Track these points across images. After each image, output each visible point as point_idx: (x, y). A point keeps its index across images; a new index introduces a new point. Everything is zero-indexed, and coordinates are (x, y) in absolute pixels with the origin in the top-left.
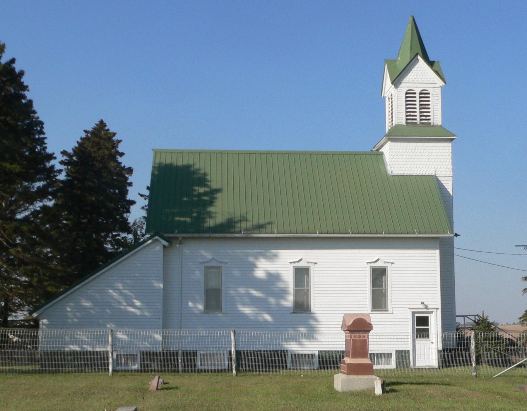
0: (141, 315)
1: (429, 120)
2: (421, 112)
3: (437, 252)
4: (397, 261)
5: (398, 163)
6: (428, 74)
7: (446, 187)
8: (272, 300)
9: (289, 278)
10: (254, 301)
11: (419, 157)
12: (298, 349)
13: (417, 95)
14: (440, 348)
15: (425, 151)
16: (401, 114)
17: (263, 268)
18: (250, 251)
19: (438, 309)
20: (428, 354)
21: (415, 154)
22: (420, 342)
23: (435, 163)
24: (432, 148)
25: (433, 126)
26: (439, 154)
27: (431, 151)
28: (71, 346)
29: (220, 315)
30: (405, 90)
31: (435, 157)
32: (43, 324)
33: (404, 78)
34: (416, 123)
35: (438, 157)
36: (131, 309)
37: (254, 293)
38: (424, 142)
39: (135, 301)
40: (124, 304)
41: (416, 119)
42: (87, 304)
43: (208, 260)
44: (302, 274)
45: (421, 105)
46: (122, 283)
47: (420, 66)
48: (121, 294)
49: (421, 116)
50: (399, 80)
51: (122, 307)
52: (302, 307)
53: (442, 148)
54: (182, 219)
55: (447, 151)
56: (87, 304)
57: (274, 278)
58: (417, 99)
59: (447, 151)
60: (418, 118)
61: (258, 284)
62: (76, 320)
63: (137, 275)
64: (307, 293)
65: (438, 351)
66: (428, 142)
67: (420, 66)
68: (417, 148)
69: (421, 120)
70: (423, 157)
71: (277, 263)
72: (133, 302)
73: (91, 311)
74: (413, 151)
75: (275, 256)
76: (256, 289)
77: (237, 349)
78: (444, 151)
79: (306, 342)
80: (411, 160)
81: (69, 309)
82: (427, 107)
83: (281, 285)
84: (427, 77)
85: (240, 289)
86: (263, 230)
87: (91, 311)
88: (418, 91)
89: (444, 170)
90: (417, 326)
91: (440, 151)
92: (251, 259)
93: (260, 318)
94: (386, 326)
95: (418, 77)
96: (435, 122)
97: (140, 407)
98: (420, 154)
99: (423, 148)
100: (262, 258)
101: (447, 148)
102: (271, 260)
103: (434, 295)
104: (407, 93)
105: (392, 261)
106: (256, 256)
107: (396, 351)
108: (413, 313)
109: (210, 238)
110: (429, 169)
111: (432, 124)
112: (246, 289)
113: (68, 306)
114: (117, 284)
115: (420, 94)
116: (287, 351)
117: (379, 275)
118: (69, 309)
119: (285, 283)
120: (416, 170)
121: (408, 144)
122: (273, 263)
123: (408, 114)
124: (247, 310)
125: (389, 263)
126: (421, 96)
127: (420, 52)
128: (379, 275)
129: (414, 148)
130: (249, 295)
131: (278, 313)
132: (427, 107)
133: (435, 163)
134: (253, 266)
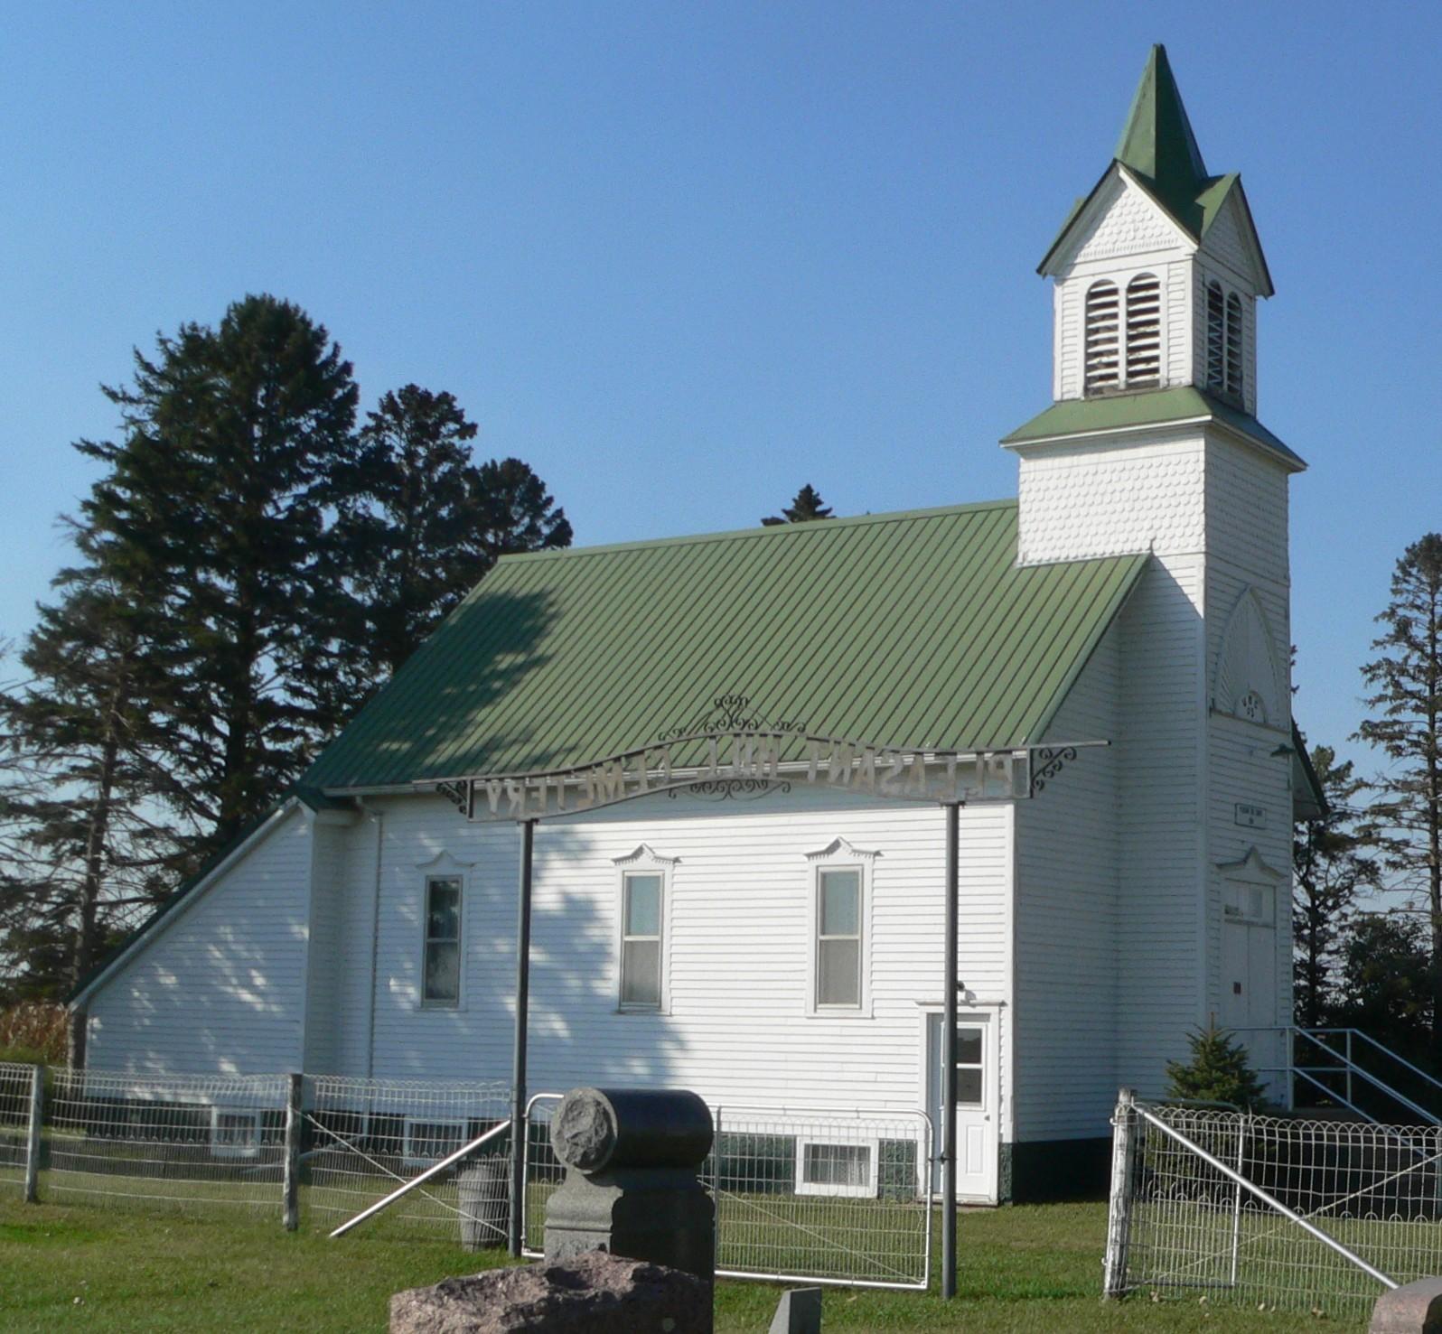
0: (264, 1011)
1: (1156, 371)
2: (1131, 350)
4: (892, 845)
5: (1042, 526)
6: (1151, 224)
7: (1186, 590)
8: (573, 982)
9: (611, 906)
13: (1121, 298)
14: (1008, 1139)
15: (1125, 475)
19: (1003, 1004)
21: (1092, 490)
23: (1152, 514)
24: (1147, 463)
25: (1166, 389)
26: (1166, 481)
27: (1143, 473)
28: (136, 1089)
29: (454, 1016)
32: (93, 1031)
34: (1114, 388)
35: (1161, 492)
36: (246, 996)
39: (254, 973)
40: (234, 981)
41: (1114, 376)
42: (170, 980)
45: (1130, 326)
46: (234, 925)
47: (1130, 201)
48: (232, 956)
49: (1130, 363)
50: (1066, 257)
51: (230, 990)
53: (1174, 459)
54: (395, 746)
55: (1190, 468)
56: (170, 980)
57: (580, 911)
58: (1122, 310)
60: (1121, 370)
65: (1001, 1145)
67: (1130, 201)
68: (1101, 468)
69: (1131, 374)
72: (251, 978)
74: (1089, 479)
78: (1180, 469)
80: (1083, 511)
83: (594, 933)
84: (1149, 232)
87: (175, 998)
88: (1122, 282)
89: (1179, 532)
91: (1170, 470)
95: (1123, 236)
96: (1172, 374)
98: (1110, 488)
99: (1119, 466)
101: (1193, 457)
104: (1091, 296)
105: (874, 848)
107: (881, 1143)
111: (1163, 383)
115: (1131, 289)
117: (838, 898)
120: (1095, 541)
121: (1075, 460)
125: (866, 853)
128: (838, 898)
133: (1152, 514)
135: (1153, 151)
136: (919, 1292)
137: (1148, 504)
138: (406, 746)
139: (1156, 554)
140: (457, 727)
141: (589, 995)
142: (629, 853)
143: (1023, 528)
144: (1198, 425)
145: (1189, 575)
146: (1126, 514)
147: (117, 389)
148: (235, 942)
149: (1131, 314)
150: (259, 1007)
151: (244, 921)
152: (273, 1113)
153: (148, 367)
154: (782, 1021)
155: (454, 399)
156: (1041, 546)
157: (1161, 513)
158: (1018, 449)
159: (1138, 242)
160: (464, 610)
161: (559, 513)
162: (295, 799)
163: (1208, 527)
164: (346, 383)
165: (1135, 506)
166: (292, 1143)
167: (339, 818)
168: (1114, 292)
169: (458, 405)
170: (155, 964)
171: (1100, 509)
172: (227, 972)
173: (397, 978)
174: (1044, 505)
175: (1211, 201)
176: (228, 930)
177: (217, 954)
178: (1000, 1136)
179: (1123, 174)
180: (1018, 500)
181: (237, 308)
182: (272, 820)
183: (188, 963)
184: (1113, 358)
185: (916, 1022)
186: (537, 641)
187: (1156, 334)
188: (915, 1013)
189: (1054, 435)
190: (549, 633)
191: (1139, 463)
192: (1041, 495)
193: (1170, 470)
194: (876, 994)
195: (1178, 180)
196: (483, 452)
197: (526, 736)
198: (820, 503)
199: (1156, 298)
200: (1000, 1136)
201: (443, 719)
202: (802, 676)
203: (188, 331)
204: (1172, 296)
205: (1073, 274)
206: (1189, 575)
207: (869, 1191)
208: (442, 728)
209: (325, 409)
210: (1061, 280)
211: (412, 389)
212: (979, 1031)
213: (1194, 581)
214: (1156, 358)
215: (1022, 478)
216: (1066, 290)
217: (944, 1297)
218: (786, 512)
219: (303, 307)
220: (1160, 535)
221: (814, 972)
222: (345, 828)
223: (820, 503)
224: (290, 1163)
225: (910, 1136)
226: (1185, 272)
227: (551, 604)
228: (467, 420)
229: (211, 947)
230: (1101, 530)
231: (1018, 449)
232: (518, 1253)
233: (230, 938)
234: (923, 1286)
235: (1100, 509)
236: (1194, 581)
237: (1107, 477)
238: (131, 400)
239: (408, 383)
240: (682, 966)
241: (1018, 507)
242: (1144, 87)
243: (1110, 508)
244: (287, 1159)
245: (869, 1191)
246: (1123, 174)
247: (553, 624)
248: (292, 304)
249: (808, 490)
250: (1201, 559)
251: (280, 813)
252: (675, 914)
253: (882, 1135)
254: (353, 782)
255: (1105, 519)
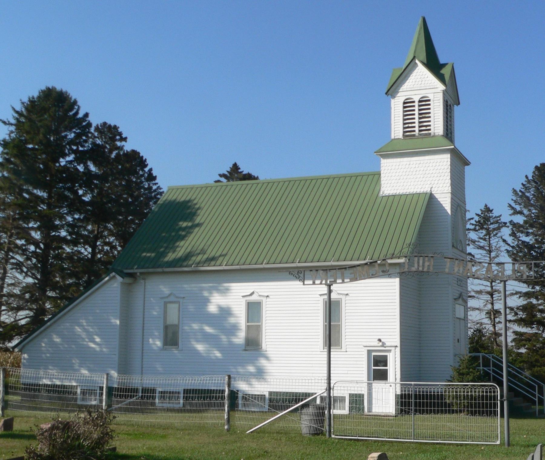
1: (430, 130)
2: (420, 122)
3: (397, 280)
5: (390, 182)
7: (444, 205)
8: (224, 338)
10: (206, 338)
11: (414, 173)
12: (247, 389)
13: (416, 104)
14: (399, 393)
15: (421, 165)
16: (398, 126)
17: (216, 302)
18: (204, 285)
19: (396, 346)
20: (384, 400)
21: (409, 170)
22: (377, 385)
23: (431, 179)
24: (429, 161)
26: (436, 168)
27: (427, 165)
28: (44, 380)
29: (176, 352)
30: (402, 100)
31: (431, 172)
32: (24, 359)
33: (401, 86)
34: (414, 135)
35: (434, 172)
36: (92, 345)
37: (208, 329)
38: (431, 155)
39: (95, 337)
40: (87, 340)
41: (414, 131)
42: (57, 340)
43: (166, 296)
44: (254, 309)
45: (420, 114)
48: (85, 330)
49: (420, 127)
50: (396, 89)
51: (85, 343)
52: (253, 344)
53: (439, 161)
54: (148, 255)
55: (445, 163)
56: (57, 340)
58: (416, 108)
59: (445, 163)
60: (417, 129)
61: (210, 319)
62: (48, 355)
63: (98, 311)
64: (258, 329)
66: (433, 154)
69: (420, 131)
70: (417, 173)
71: (229, 297)
72: (94, 339)
73: (61, 346)
74: (407, 166)
75: (227, 289)
76: (209, 325)
77: (110, 385)
79: (254, 382)
81: (44, 345)
82: (427, 115)
83: (232, 320)
84: (426, 82)
85: (194, 325)
86: (213, 263)
88: (416, 99)
89: (441, 185)
90: (374, 366)
91: (437, 164)
92: (206, 294)
93: (212, 355)
94: (340, 366)
95: (417, 83)
96: (435, 131)
97: (389, 454)
98: (415, 170)
99: (419, 162)
100: (214, 292)
101: (446, 160)
102: (224, 295)
103: (392, 330)
104: (404, 103)
105: (346, 293)
106: (211, 290)
107: (350, 394)
108: (369, 352)
109: (164, 273)
110: (424, 186)
111: (432, 134)
112: (199, 325)
113: (43, 342)
114: (81, 321)
115: (420, 101)
116: (238, 391)
117: (332, 309)
118: (44, 345)
119: (238, 319)
121: (402, 159)
122: (225, 297)
123: (407, 126)
124: (200, 347)
126: (420, 104)
127: (423, 55)
128: (332, 309)
129: (408, 163)
130: (202, 331)
131: (230, 350)
132: (427, 115)
133: (431, 179)
134: (207, 301)
135: (425, 54)
136: (497, 445)
137: (429, 176)
138: (153, 255)
139: (433, 193)
140: (174, 249)
141: (231, 343)
142: (249, 294)
143: (382, 182)
144: (448, 149)
145: (445, 201)
146: (421, 179)
147: (6, 120)
148: (87, 326)
149: (420, 110)
150: (98, 349)
151: (90, 318)
152: (151, 389)
153: (17, 112)
154: (311, 353)
155: (119, 127)
156: (389, 189)
157: (434, 179)
158: (380, 155)
159: (422, 85)
160: (159, 206)
161: (151, 170)
162: (114, 274)
163: (451, 184)
164: (86, 121)
165: (422, 176)
166: (228, 400)
167: (128, 280)
168: (414, 102)
169: (120, 130)
170: (52, 334)
171: (412, 177)
172: (84, 336)
173: (152, 338)
174: (390, 175)
175: (446, 71)
176: (84, 321)
177: (79, 330)
178: (396, 391)
179: (417, 61)
180: (380, 172)
181: (43, 91)
182: (103, 281)
183: (66, 333)
184: (413, 125)
185: (363, 353)
186: (195, 217)
187: (430, 117)
188: (363, 350)
189: (393, 150)
190: (199, 215)
191: (426, 161)
192: (389, 171)
193: (437, 164)
194: (347, 343)
195: (434, 65)
196: (128, 147)
197: (203, 252)
198: (239, 169)
199: (429, 105)
200: (396, 391)
201: (165, 245)
202: (325, 234)
203: (31, 99)
204: (435, 104)
205: (398, 95)
206: (445, 201)
207: (346, 412)
208: (166, 248)
209: (79, 129)
210: (394, 97)
211: (105, 123)
212: (386, 356)
213: (447, 202)
214: (430, 126)
215: (382, 165)
216: (395, 101)
217: (506, 446)
218: (228, 171)
219: (69, 92)
220: (434, 186)
221: (320, 337)
222: (130, 284)
223: (239, 169)
224: (228, 407)
225: (362, 393)
226: (440, 97)
227: (196, 204)
228: (124, 136)
229: (77, 327)
230: (412, 183)
231: (380, 155)
232: (330, 436)
233: (85, 324)
234: (498, 443)
235: (412, 177)
236: (447, 202)
237: (414, 166)
238: (12, 124)
239: (104, 121)
240: (270, 334)
241: (380, 174)
242: (420, 31)
243: (415, 177)
244: (226, 406)
245: (346, 412)
246: (417, 61)
247: (199, 211)
248: (64, 90)
249: (235, 165)
250: (450, 195)
251: (107, 279)
252: (267, 315)
253: (269, 390)
254: (136, 267)
255: (413, 180)
